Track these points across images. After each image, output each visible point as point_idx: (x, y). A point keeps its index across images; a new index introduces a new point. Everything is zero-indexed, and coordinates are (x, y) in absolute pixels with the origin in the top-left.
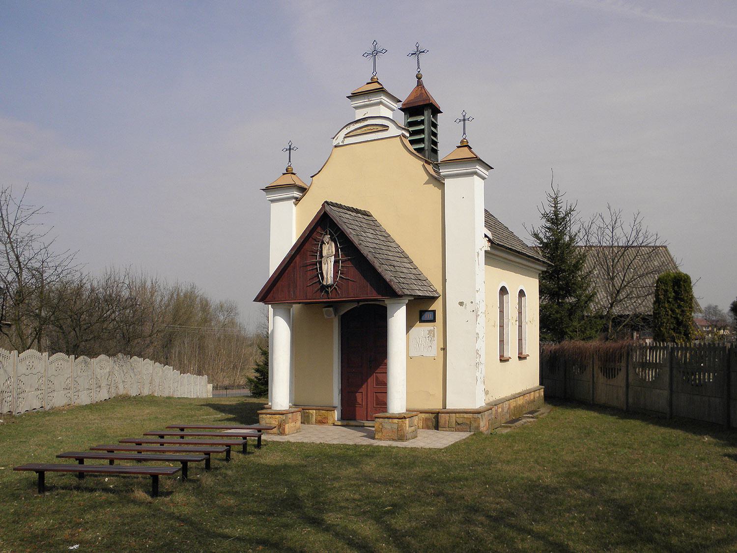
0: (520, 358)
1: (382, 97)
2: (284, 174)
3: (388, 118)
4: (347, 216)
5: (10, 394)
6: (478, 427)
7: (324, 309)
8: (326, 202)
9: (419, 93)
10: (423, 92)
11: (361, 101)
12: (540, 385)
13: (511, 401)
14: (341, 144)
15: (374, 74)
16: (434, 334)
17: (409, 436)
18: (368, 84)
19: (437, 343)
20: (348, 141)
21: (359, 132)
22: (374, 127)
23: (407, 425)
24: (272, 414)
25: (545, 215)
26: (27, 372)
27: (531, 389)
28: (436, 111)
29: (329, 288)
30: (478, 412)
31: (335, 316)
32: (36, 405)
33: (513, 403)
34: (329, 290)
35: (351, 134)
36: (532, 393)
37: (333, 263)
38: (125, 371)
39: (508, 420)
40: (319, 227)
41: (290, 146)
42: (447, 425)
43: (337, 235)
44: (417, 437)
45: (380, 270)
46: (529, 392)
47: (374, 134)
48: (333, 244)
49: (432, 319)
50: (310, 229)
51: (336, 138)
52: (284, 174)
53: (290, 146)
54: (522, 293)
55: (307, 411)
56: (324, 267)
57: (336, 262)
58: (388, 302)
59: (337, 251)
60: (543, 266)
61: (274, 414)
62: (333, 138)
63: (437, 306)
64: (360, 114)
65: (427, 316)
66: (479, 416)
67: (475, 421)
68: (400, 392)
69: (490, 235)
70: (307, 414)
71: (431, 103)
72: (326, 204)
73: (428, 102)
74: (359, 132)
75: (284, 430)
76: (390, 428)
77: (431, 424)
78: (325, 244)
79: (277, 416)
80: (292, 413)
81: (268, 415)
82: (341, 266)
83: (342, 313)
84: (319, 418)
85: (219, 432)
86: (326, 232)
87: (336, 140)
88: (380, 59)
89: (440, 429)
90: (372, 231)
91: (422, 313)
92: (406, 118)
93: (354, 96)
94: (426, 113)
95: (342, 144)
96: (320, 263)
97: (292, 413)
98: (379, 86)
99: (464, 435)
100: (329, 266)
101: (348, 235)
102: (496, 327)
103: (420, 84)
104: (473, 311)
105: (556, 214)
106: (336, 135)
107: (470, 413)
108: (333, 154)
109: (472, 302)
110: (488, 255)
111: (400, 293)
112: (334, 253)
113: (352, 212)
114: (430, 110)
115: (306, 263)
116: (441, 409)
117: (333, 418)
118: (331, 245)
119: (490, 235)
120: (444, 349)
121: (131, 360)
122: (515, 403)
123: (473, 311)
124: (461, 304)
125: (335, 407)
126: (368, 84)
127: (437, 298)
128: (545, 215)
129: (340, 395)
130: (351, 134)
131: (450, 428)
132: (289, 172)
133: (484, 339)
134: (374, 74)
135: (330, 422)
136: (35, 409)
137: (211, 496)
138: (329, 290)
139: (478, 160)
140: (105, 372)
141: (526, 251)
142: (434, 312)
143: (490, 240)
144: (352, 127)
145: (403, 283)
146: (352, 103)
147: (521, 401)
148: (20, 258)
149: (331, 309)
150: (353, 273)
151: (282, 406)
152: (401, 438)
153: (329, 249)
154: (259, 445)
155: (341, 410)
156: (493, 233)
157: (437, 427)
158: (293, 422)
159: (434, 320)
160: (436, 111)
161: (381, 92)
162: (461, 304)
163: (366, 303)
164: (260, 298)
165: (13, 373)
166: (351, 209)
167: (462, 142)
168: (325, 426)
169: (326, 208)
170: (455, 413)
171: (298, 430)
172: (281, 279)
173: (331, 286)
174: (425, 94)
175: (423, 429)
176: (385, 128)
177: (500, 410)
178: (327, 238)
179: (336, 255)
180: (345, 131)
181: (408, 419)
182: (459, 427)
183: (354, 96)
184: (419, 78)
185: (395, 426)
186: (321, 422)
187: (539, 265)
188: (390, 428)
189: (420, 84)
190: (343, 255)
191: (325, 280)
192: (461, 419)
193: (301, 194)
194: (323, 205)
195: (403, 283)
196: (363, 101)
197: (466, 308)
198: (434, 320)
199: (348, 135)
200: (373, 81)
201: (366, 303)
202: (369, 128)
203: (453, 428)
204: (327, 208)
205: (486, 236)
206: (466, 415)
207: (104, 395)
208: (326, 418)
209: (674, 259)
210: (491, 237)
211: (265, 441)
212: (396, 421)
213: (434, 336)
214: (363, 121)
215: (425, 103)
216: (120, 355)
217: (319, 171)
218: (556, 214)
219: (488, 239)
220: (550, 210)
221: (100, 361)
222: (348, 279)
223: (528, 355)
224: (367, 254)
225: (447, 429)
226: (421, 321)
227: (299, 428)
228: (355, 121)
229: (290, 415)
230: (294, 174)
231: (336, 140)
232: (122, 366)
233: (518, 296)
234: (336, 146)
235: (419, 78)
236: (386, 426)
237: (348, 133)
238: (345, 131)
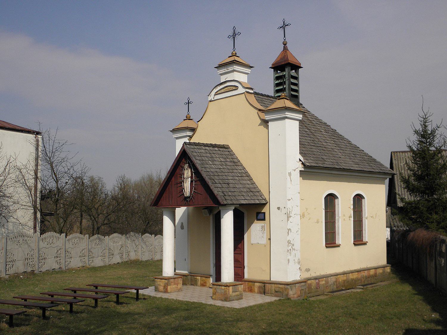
1: (234, 67)
2: (184, 120)
3: (237, 81)
5: (32, 260)
6: (287, 295)
9: (283, 56)
11: (223, 70)
14: (213, 99)
16: (265, 228)
18: (229, 57)
19: (265, 236)
21: (223, 91)
22: (231, 87)
24: (161, 279)
25: (416, 132)
26: (47, 246)
28: (296, 67)
30: (287, 284)
32: (56, 266)
34: (188, 200)
35: (219, 92)
37: (190, 182)
38: (137, 244)
40: (184, 159)
41: (189, 101)
42: (270, 291)
45: (212, 188)
47: (233, 92)
48: (190, 170)
49: (263, 218)
51: (210, 95)
52: (184, 120)
53: (189, 101)
55: (196, 277)
56: (185, 185)
57: (192, 182)
59: (192, 174)
61: (162, 279)
62: (209, 96)
63: (265, 210)
64: (223, 79)
65: (261, 216)
66: (288, 287)
67: (285, 290)
68: (227, 268)
69: (302, 159)
70: (196, 279)
72: (184, 144)
73: (287, 62)
74: (223, 91)
75: (167, 289)
76: (220, 292)
77: (262, 290)
79: (163, 280)
80: (174, 279)
81: (159, 280)
82: (194, 184)
84: (202, 282)
85: (43, 295)
86: (186, 162)
87: (210, 97)
88: (287, 28)
89: (266, 294)
91: (258, 213)
92: (275, 73)
93: (220, 66)
94: (287, 70)
97: (174, 279)
100: (188, 185)
103: (285, 49)
104: (286, 214)
105: (425, 131)
106: (210, 94)
107: (281, 284)
108: (209, 107)
109: (285, 208)
110: (303, 173)
111: (222, 203)
112: (190, 176)
114: (290, 68)
115: (177, 182)
116: (268, 280)
117: (209, 282)
118: (188, 171)
119: (302, 159)
120: (270, 239)
121: (143, 237)
123: (286, 214)
124: (279, 208)
125: (211, 276)
126: (229, 57)
127: (267, 203)
128: (416, 132)
129: (215, 267)
130: (219, 92)
131: (272, 294)
132: (188, 118)
135: (208, 285)
136: (41, 271)
137: (327, 323)
138: (188, 200)
140: (118, 245)
142: (264, 213)
143: (303, 163)
144: (219, 88)
146: (218, 71)
147: (355, 276)
150: (201, 189)
151: (168, 274)
152: (226, 299)
153: (187, 173)
154: (137, 298)
155: (216, 278)
157: (264, 293)
158: (175, 284)
159: (264, 219)
162: (279, 208)
164: (153, 204)
165: (35, 247)
168: (195, 287)
170: (274, 284)
171: (180, 290)
172: (165, 192)
173: (189, 197)
174: (287, 56)
175: (257, 293)
178: (186, 166)
179: (191, 177)
180: (215, 91)
181: (231, 288)
182: (276, 293)
183: (220, 66)
184: (285, 44)
185: (223, 291)
186: (203, 285)
188: (220, 292)
189: (285, 49)
190: (196, 177)
192: (278, 288)
193: (192, 133)
194: (183, 145)
196: (224, 70)
197: (281, 211)
198: (264, 219)
202: (228, 88)
203: (273, 294)
205: (300, 160)
206: (280, 286)
207: (117, 259)
208: (205, 282)
211: (143, 295)
212: (223, 287)
213: (264, 230)
214: (224, 83)
215: (286, 63)
216: (132, 233)
217: (202, 118)
218: (425, 131)
219: (301, 163)
220: (419, 128)
221: (113, 238)
222: (198, 193)
223: (367, 242)
224: (205, 177)
225: (270, 295)
226: (258, 220)
227: (180, 289)
228: (220, 84)
229: (172, 280)
230: (192, 120)
231: (210, 97)
232: (134, 241)
234: (210, 101)
235: (285, 44)
236: (219, 291)
237: (217, 92)
238: (215, 91)
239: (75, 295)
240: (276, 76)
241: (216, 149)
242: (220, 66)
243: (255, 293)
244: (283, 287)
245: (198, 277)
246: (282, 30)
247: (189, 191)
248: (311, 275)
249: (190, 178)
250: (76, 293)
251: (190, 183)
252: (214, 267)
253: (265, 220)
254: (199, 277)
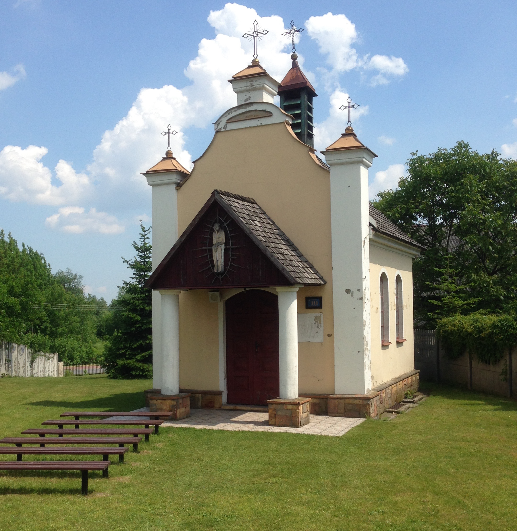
0: (398, 343)
4: (236, 204)
7: (209, 293)
8: (216, 190)
9: (294, 75)
10: (299, 74)
12: (415, 369)
13: (393, 386)
14: (223, 130)
15: (256, 56)
16: (321, 319)
17: (302, 421)
20: (231, 126)
21: (241, 117)
23: (301, 411)
27: (408, 373)
29: (220, 276)
31: (221, 301)
33: (394, 388)
35: (233, 120)
36: (410, 378)
39: (391, 406)
41: (169, 130)
43: (227, 223)
44: (309, 422)
46: (407, 376)
50: (200, 216)
53: (169, 130)
54: (398, 279)
58: (280, 291)
60: (417, 251)
69: (374, 223)
71: (308, 86)
72: (216, 193)
78: (215, 232)
83: (227, 298)
90: (258, 219)
95: (224, 130)
96: (211, 251)
98: (260, 71)
99: (356, 422)
101: (239, 224)
102: (378, 312)
113: (239, 200)
119: (374, 223)
122: (396, 387)
129: (226, 379)
130: (233, 120)
133: (370, 326)
134: (256, 56)
135: (217, 405)
139: (363, 148)
141: (404, 237)
145: (294, 272)
148: (469, 439)
149: (217, 293)
156: (378, 222)
160: (311, 94)
161: (264, 77)
162: (348, 291)
163: (252, 289)
166: (252, 200)
167: (347, 129)
169: (216, 197)
176: (269, 114)
177: (384, 395)
178: (216, 227)
179: (226, 244)
187: (414, 250)
191: (216, 267)
195: (294, 272)
197: (352, 295)
199: (228, 122)
200: (255, 64)
201: (252, 289)
204: (217, 196)
209: (178, 169)
210: (375, 226)
219: (372, 228)
233: (395, 282)
239: (61, 431)
240: (284, 104)
241: (246, 203)
242: (236, 80)
243: (493, 409)
244: (361, 403)
245: (197, 395)
246: (250, 41)
247: (223, 264)
248: (379, 384)
249: (224, 245)
250: (78, 428)
251: (224, 252)
252: (225, 379)
253: (322, 308)
254: (200, 395)
